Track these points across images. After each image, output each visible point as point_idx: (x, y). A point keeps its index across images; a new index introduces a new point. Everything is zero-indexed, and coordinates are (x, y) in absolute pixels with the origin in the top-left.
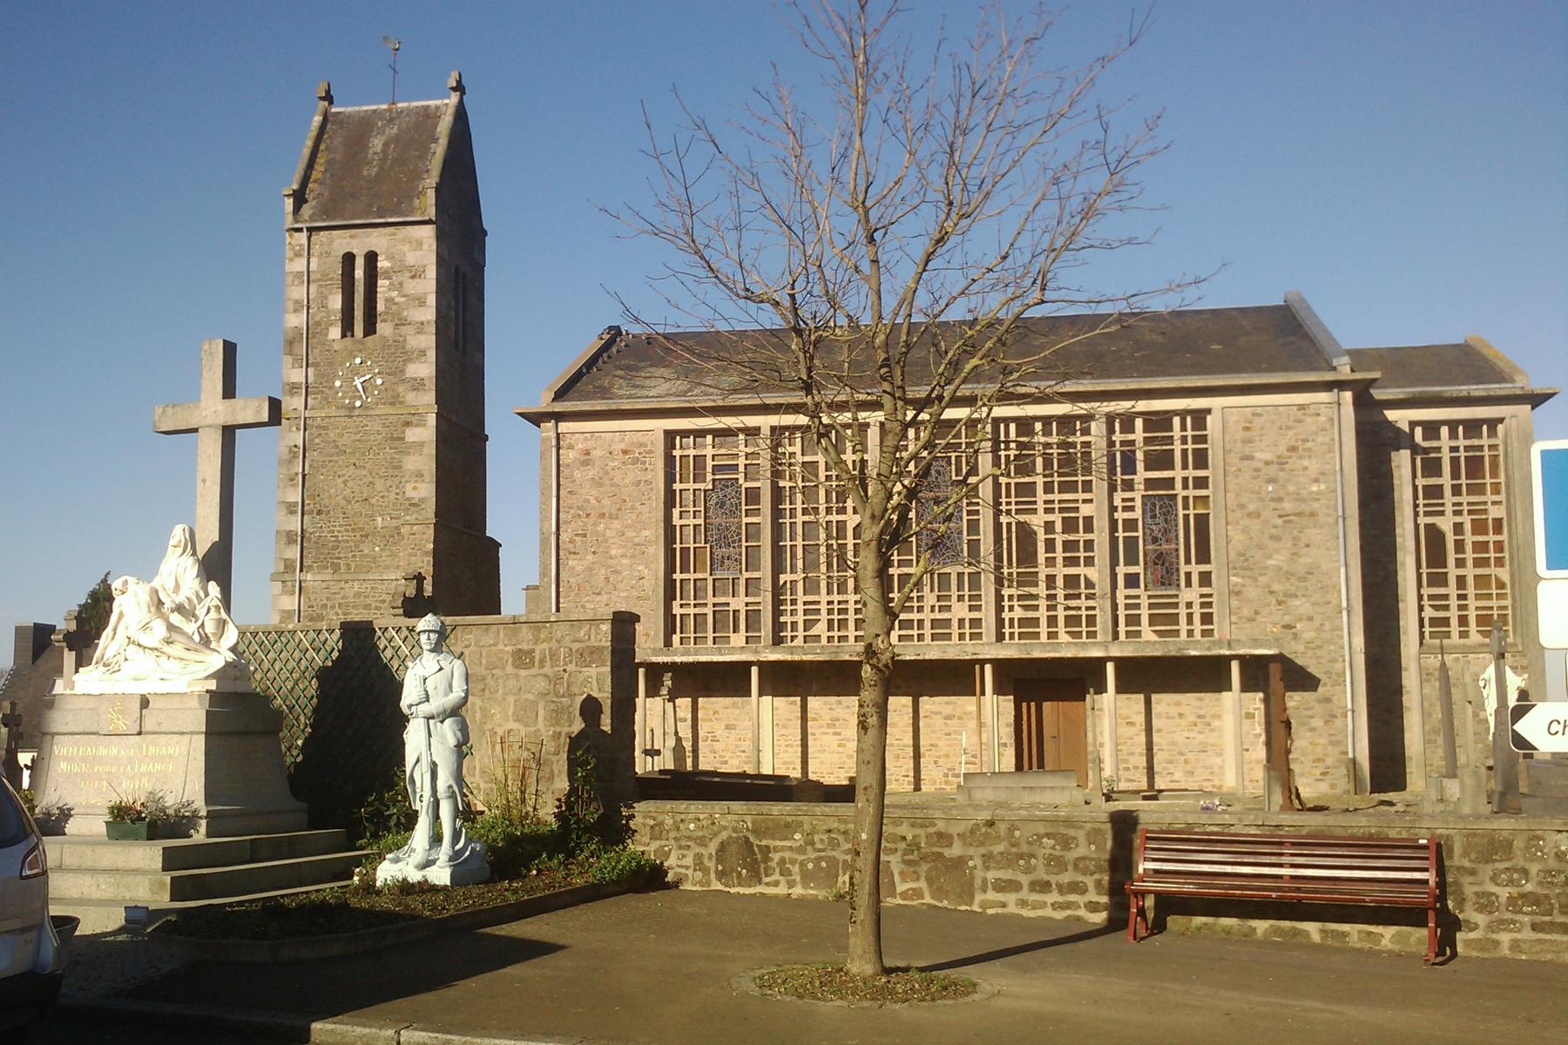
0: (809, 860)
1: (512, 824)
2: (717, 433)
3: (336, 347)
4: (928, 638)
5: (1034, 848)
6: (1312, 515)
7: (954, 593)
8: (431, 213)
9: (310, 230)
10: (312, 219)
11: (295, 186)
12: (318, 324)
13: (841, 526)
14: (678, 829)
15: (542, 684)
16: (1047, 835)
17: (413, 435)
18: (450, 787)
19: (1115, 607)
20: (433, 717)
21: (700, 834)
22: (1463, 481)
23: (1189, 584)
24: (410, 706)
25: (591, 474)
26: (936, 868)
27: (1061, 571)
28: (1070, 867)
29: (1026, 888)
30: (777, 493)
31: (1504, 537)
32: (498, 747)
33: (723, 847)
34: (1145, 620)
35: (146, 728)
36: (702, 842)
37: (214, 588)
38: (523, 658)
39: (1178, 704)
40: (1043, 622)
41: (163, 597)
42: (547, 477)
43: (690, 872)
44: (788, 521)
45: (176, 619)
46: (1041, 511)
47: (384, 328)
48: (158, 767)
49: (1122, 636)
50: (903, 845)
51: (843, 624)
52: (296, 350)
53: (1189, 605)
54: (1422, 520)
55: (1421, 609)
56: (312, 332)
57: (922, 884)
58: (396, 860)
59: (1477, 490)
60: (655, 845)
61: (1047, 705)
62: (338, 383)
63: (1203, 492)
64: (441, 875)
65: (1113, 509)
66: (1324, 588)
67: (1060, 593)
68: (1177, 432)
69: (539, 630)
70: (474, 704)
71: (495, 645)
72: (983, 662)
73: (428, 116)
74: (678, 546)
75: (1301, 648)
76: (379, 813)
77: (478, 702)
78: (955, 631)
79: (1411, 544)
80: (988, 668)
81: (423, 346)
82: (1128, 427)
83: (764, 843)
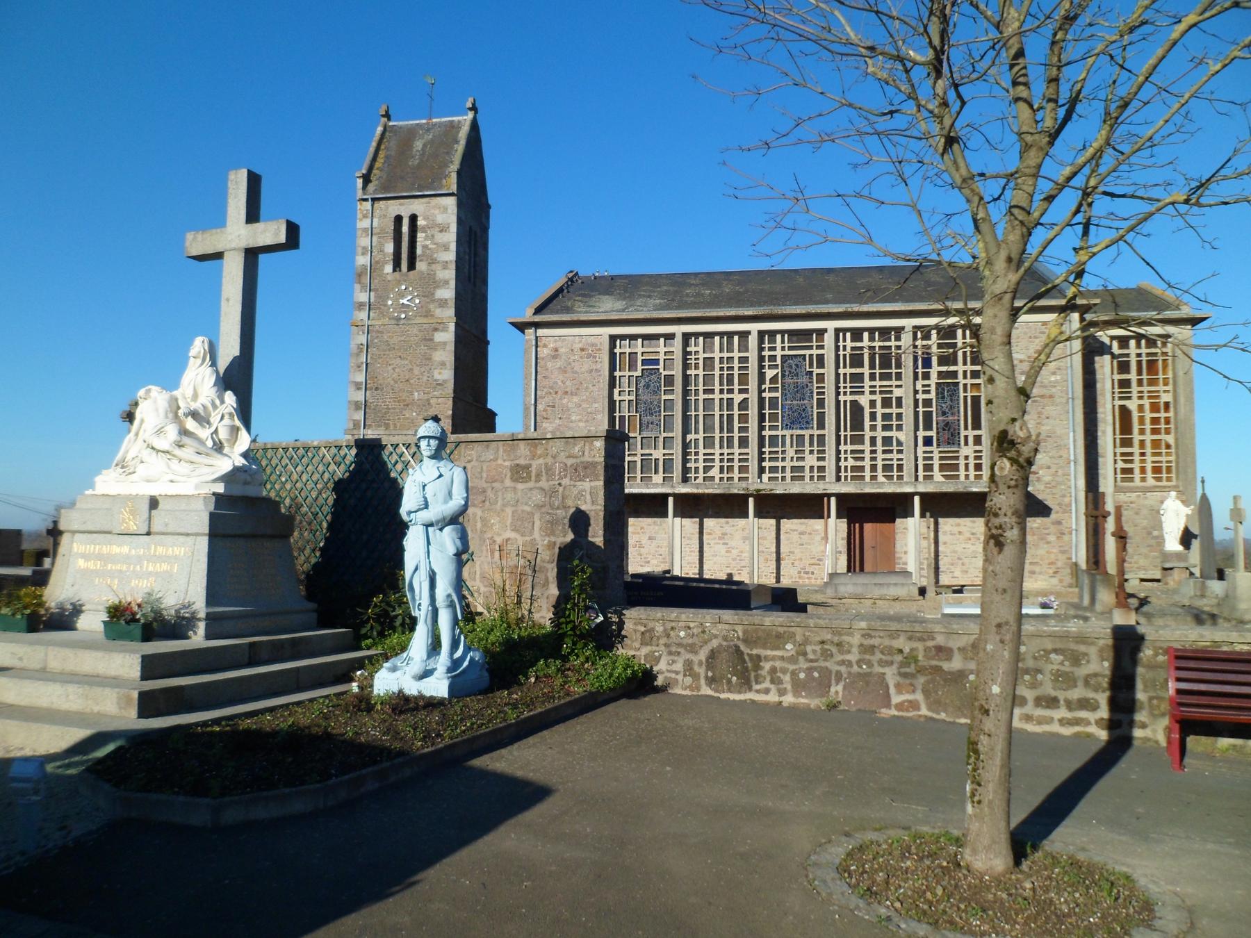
0: (800, 670)
1: (509, 626)
2: (646, 337)
3: (389, 278)
4: (788, 479)
5: (1041, 664)
6: (1051, 397)
7: (807, 448)
8: (454, 188)
9: (374, 200)
10: (375, 192)
11: (364, 171)
12: (377, 262)
13: (730, 401)
14: (668, 636)
15: (538, 497)
16: (1055, 651)
17: (440, 337)
18: (449, 596)
19: (916, 459)
20: (431, 525)
21: (690, 641)
22: (1145, 376)
23: (966, 443)
24: (409, 513)
25: (559, 365)
26: (933, 681)
27: (880, 434)
28: (1080, 683)
29: (1031, 703)
30: (686, 378)
31: (1171, 414)
32: (497, 554)
33: (713, 655)
34: (936, 468)
35: (154, 529)
36: (692, 649)
37: (230, 398)
38: (520, 473)
39: (958, 525)
40: (868, 469)
41: (181, 404)
42: (527, 367)
43: (680, 677)
44: (693, 398)
45: (191, 424)
47: (421, 266)
48: (165, 567)
49: (921, 478)
50: (899, 658)
51: (730, 469)
52: (363, 281)
53: (967, 458)
55: (1115, 462)
56: (374, 267)
57: (919, 696)
58: (394, 669)
59: (1152, 382)
60: (645, 651)
61: (868, 527)
62: (390, 302)
63: (977, 381)
64: (438, 687)
65: (916, 392)
66: (1059, 447)
68: (959, 341)
69: (536, 447)
70: (475, 515)
71: (496, 459)
72: (829, 496)
73: (453, 127)
74: (617, 414)
75: (1042, 487)
76: (385, 614)
77: (479, 513)
78: (807, 474)
79: (1110, 418)
80: (833, 500)
81: (447, 277)
82: (927, 336)
83: (755, 652)
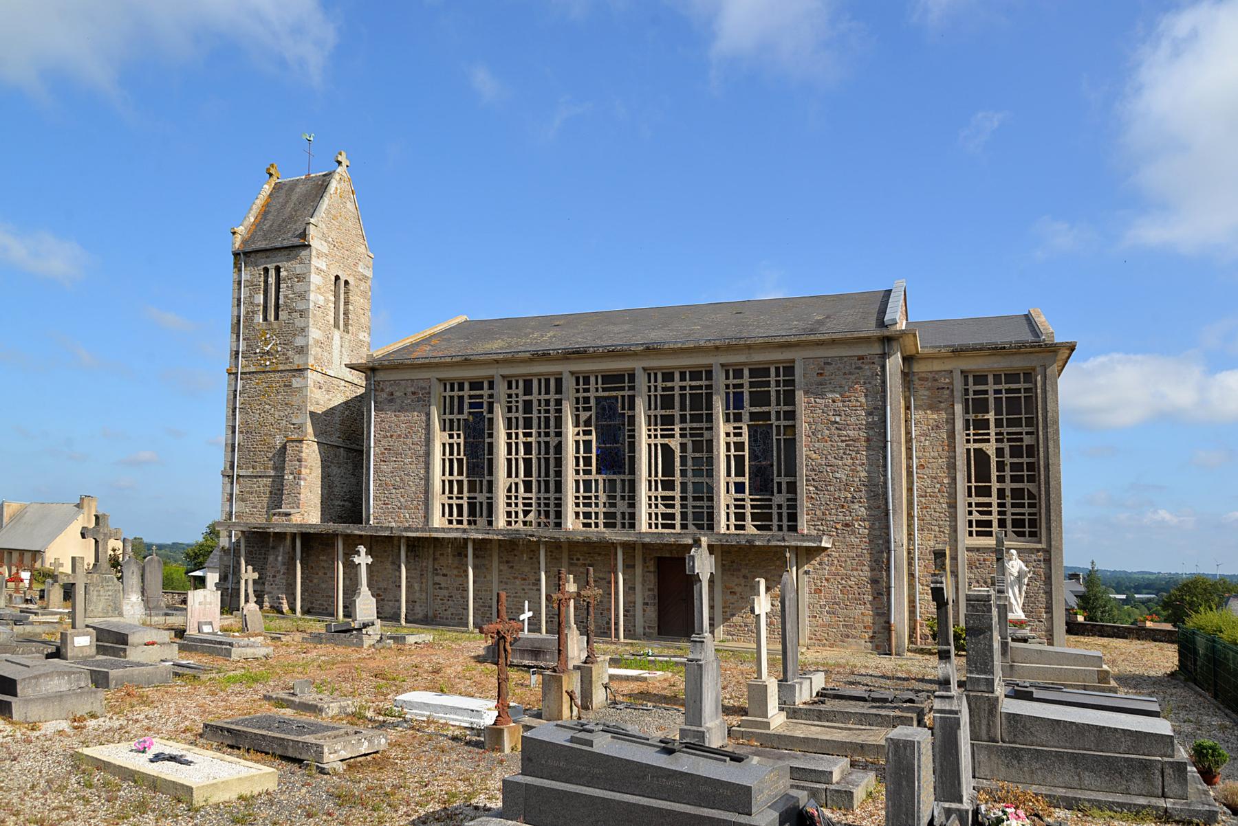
23: (780, 492)
34: (749, 517)
46: (677, 435)
47: (283, 315)
53: (780, 507)
54: (973, 446)
67: (1009, 501)
